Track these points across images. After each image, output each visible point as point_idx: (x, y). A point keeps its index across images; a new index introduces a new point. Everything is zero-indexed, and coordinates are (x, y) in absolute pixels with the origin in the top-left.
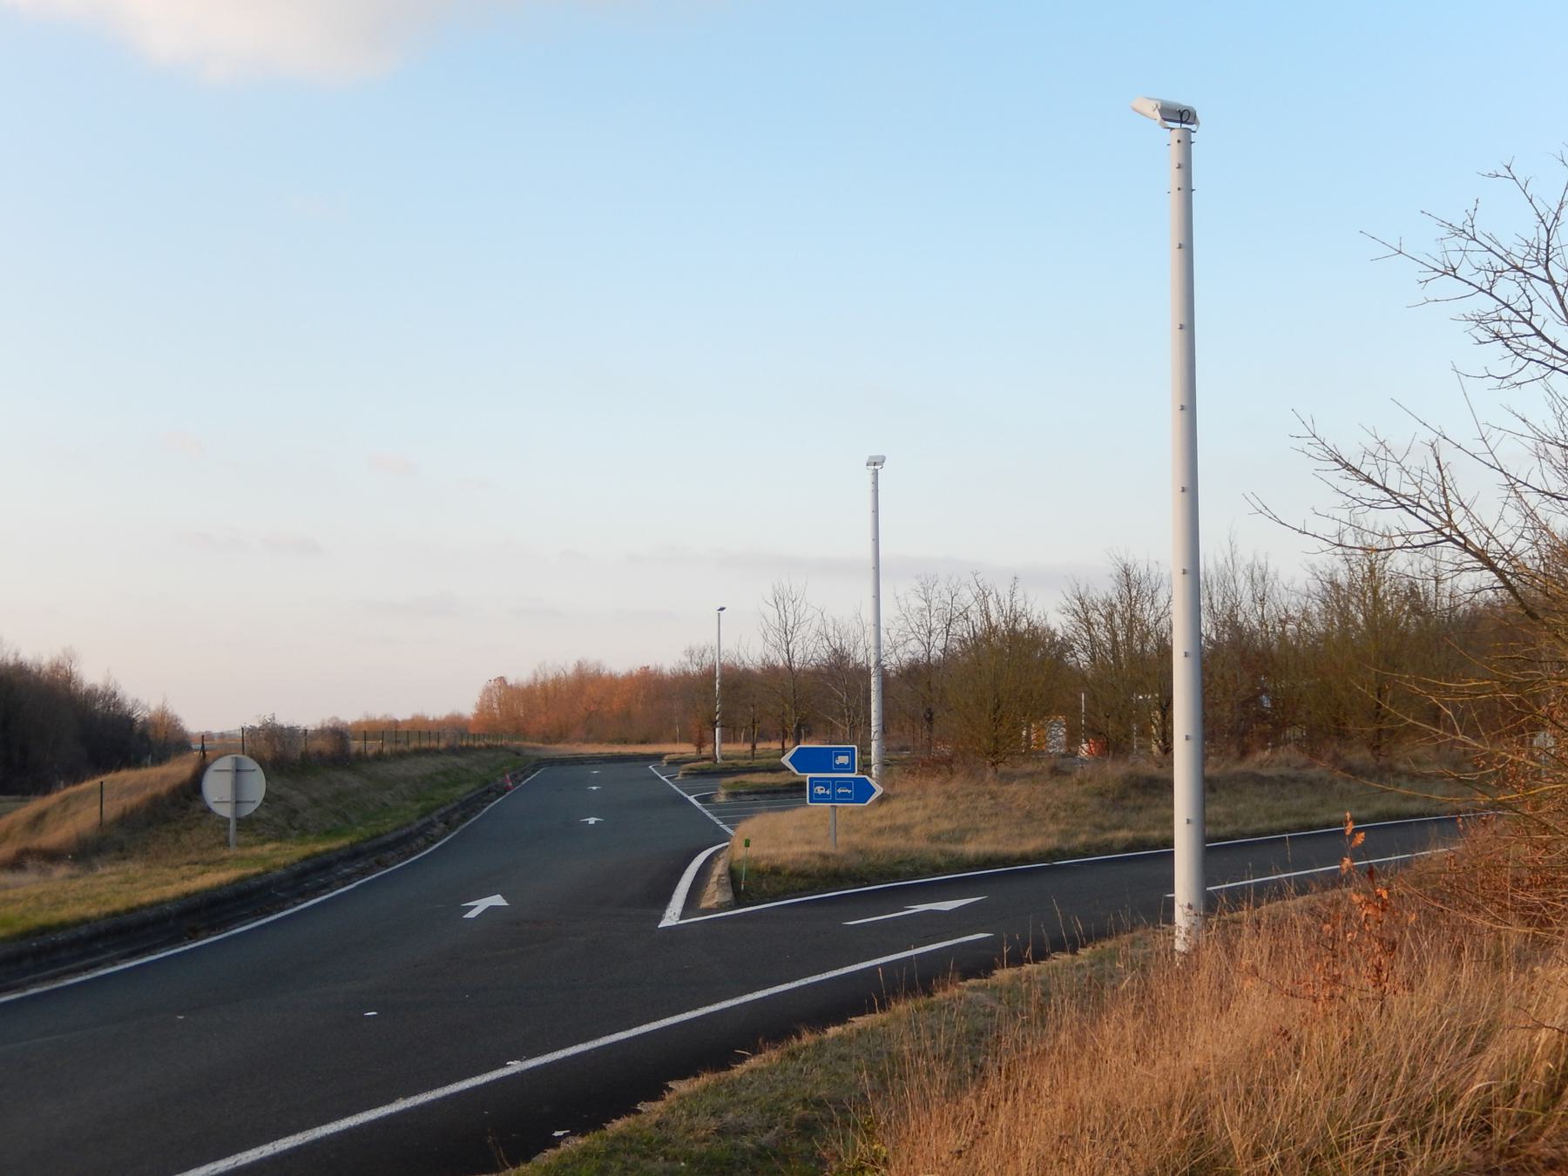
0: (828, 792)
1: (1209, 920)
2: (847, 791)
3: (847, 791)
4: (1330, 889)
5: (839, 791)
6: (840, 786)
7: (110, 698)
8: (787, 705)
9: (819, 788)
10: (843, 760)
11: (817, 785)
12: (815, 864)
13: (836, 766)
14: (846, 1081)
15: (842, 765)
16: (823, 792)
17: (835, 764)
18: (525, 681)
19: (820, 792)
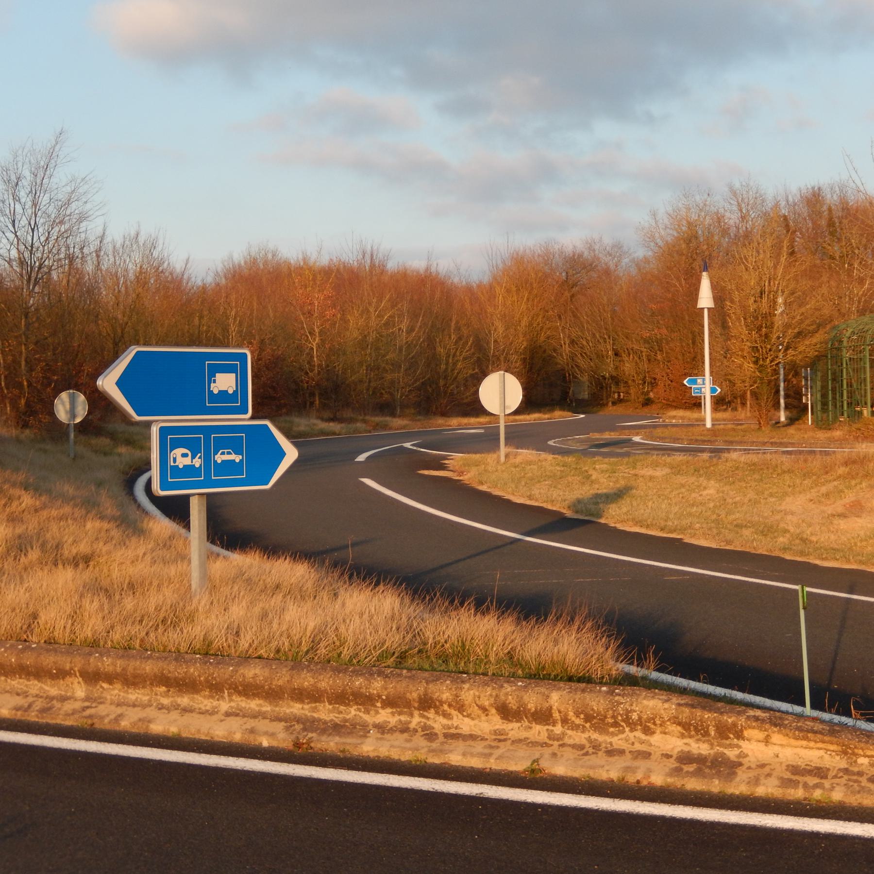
0: (197, 462)
1: (499, 485)
2: (232, 457)
3: (232, 457)
4: (860, 440)
5: (219, 458)
6: (221, 445)
7: (472, 767)
8: (234, 310)
9: (179, 452)
10: (225, 382)
11: (176, 445)
12: (738, 228)
13: (213, 397)
14: (621, 712)
15: (223, 393)
16: (187, 461)
17: (211, 392)
18: (199, 283)
19: (182, 462)
